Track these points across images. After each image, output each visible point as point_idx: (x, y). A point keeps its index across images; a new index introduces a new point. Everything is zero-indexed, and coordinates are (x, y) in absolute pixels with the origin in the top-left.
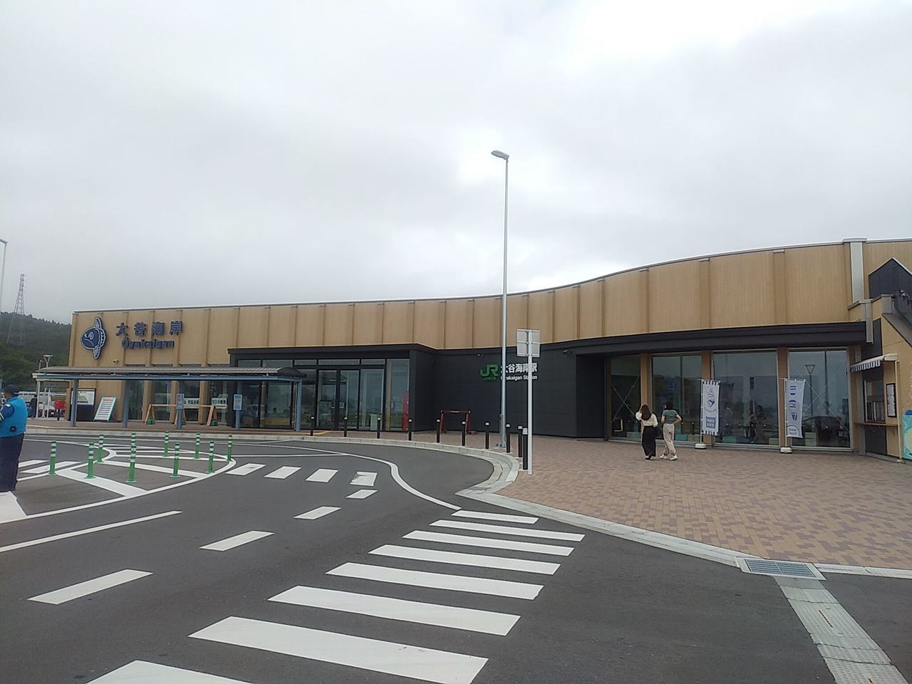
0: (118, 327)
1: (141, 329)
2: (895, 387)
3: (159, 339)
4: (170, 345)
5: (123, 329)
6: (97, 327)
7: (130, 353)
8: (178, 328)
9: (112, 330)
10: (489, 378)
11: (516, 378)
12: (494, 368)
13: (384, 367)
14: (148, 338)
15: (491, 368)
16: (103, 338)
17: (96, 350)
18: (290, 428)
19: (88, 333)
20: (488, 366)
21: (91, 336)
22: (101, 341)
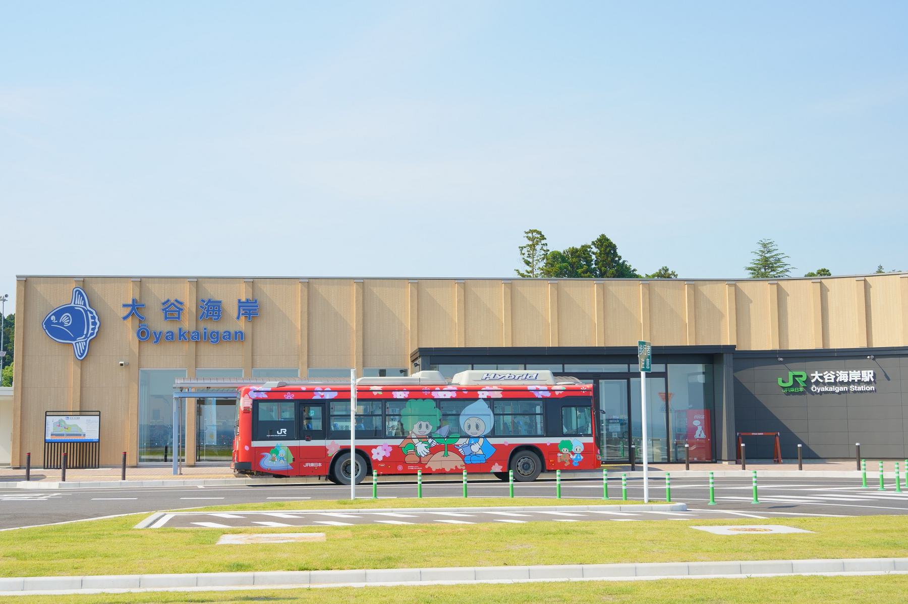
0: (124, 306)
1: (172, 310)
2: (162, 460)
3: (211, 327)
4: (239, 336)
5: (136, 309)
6: (79, 304)
7: (150, 349)
8: (250, 309)
9: (115, 304)
10: (792, 390)
11: (838, 389)
12: (801, 376)
13: (664, 375)
14: (188, 324)
15: (794, 376)
16: (94, 324)
17: (80, 343)
18: (714, 457)
19: (58, 314)
20: (791, 374)
21: (66, 319)
22: (89, 329)
